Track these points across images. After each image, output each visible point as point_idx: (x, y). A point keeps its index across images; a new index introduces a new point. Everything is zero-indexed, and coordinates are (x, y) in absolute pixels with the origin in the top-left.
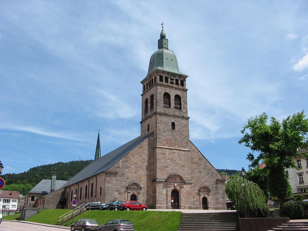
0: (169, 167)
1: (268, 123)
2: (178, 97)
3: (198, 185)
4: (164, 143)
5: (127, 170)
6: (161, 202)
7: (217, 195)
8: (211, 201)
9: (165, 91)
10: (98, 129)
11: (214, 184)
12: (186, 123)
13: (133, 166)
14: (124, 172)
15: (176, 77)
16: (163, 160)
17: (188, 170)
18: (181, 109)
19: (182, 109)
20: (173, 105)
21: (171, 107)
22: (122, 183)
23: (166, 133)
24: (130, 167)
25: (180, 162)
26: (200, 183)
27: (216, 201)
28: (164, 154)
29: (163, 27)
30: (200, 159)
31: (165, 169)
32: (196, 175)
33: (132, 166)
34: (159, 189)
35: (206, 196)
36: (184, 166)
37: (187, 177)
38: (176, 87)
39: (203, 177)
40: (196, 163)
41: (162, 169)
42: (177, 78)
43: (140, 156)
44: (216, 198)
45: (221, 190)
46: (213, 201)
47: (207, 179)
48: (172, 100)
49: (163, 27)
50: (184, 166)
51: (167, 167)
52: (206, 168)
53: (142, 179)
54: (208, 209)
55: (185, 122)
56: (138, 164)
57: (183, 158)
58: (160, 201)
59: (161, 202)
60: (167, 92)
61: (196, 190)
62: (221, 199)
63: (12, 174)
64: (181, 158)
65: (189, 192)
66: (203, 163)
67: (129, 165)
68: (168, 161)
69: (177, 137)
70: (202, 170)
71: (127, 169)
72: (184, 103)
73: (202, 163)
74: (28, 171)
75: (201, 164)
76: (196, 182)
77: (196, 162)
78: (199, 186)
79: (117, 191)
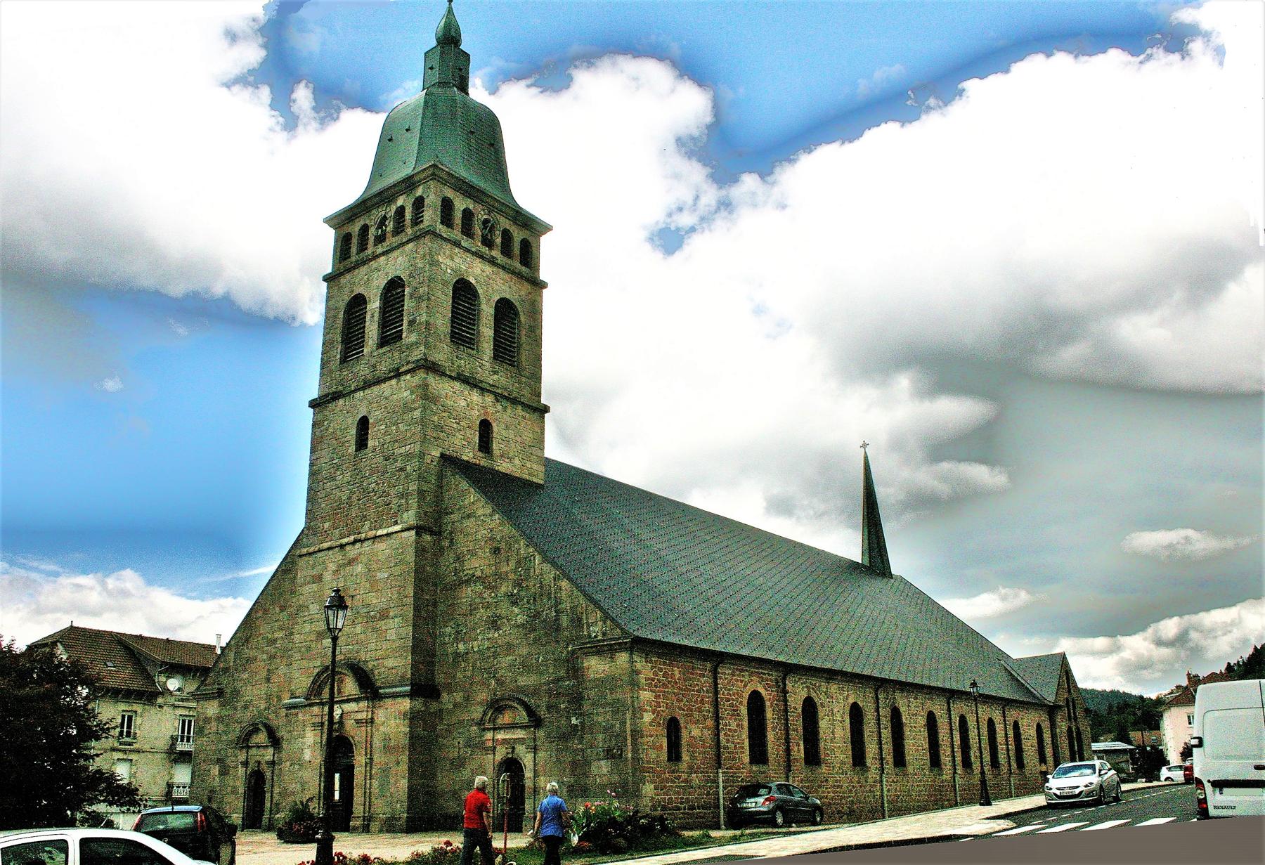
5: (245, 676)
7: (575, 744)
36: (384, 615)
65: (393, 743)
67: (252, 653)
77: (478, 573)
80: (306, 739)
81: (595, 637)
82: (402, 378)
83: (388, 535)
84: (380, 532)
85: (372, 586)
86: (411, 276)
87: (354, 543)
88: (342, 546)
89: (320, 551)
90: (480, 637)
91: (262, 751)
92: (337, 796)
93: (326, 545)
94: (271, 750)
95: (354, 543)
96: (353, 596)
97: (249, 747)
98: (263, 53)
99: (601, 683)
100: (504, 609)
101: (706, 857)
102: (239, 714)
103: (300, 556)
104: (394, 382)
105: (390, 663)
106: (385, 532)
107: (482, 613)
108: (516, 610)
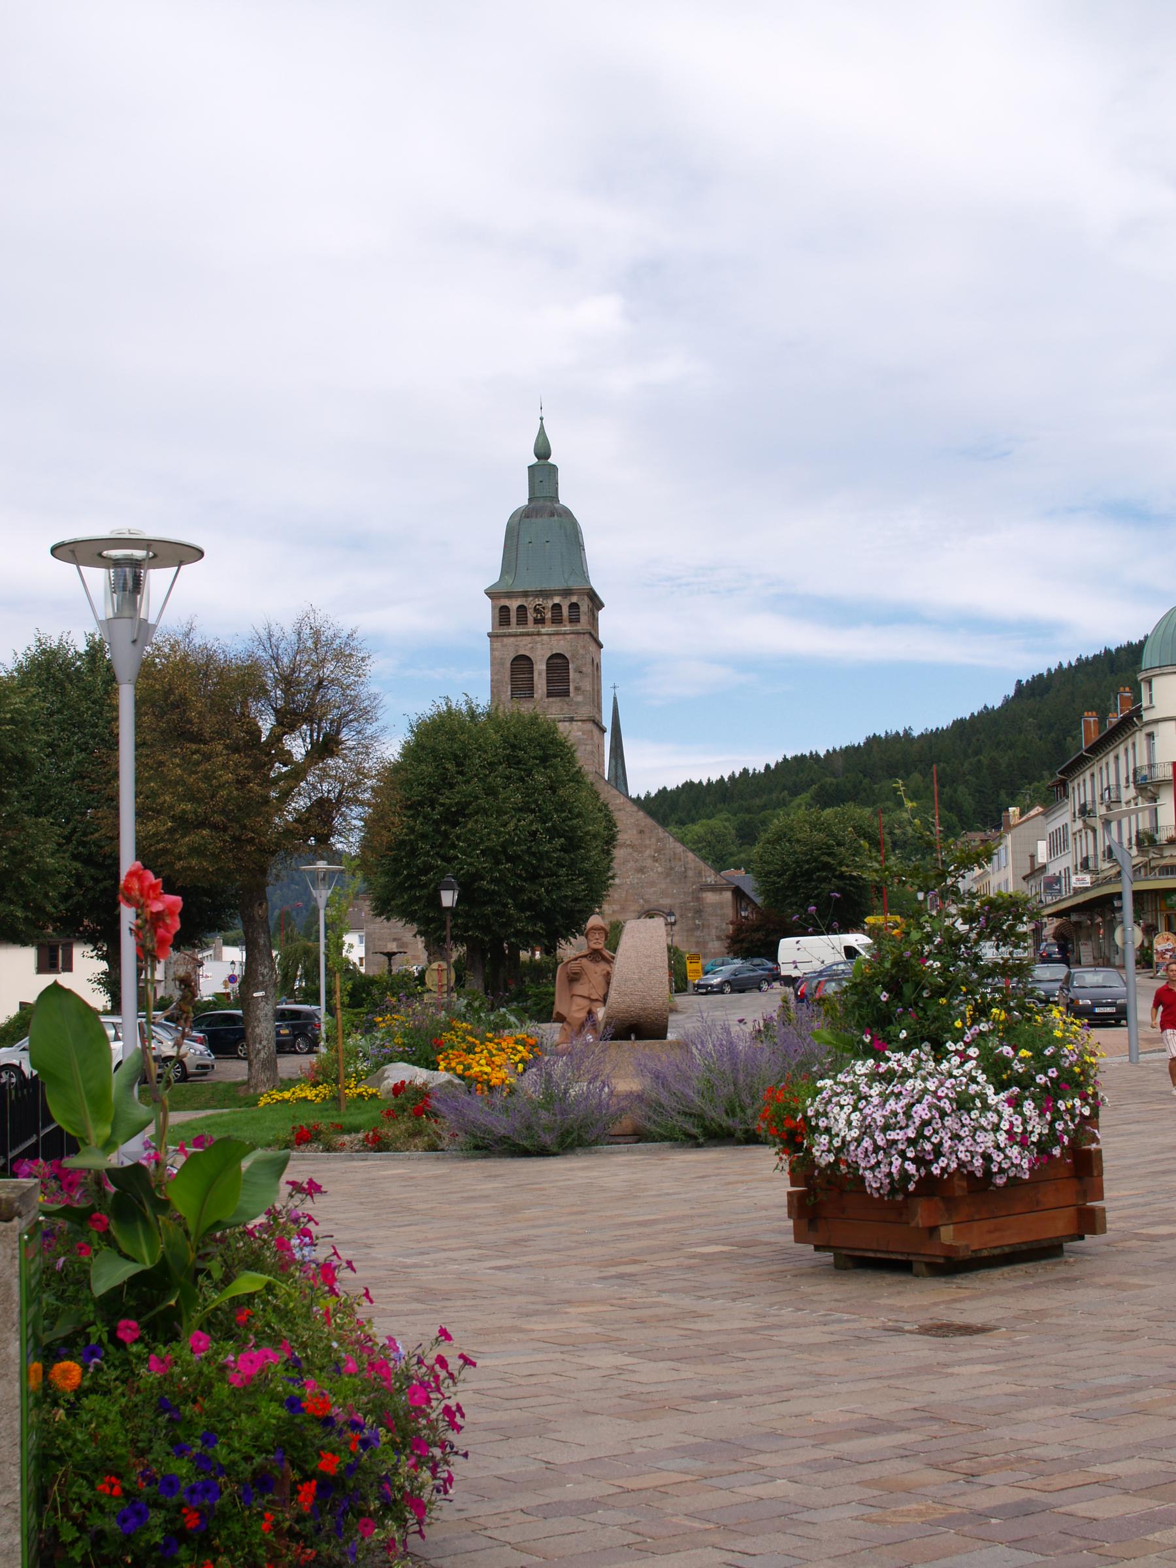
2: (558, 664)
9: (517, 651)
10: (612, 685)
11: (690, 899)
12: (583, 734)
18: (566, 693)
19: (571, 695)
21: (535, 696)
26: (641, 901)
30: (641, 832)
39: (653, 884)
40: (629, 845)
42: (557, 600)
45: (716, 915)
47: (664, 886)
48: (540, 674)
49: (542, 419)
52: (662, 856)
55: (580, 733)
62: (715, 943)
63: (822, 754)
66: (654, 840)
72: (578, 675)
73: (647, 842)
74: (1008, 702)
76: (626, 901)
77: (628, 842)
79: (394, 940)
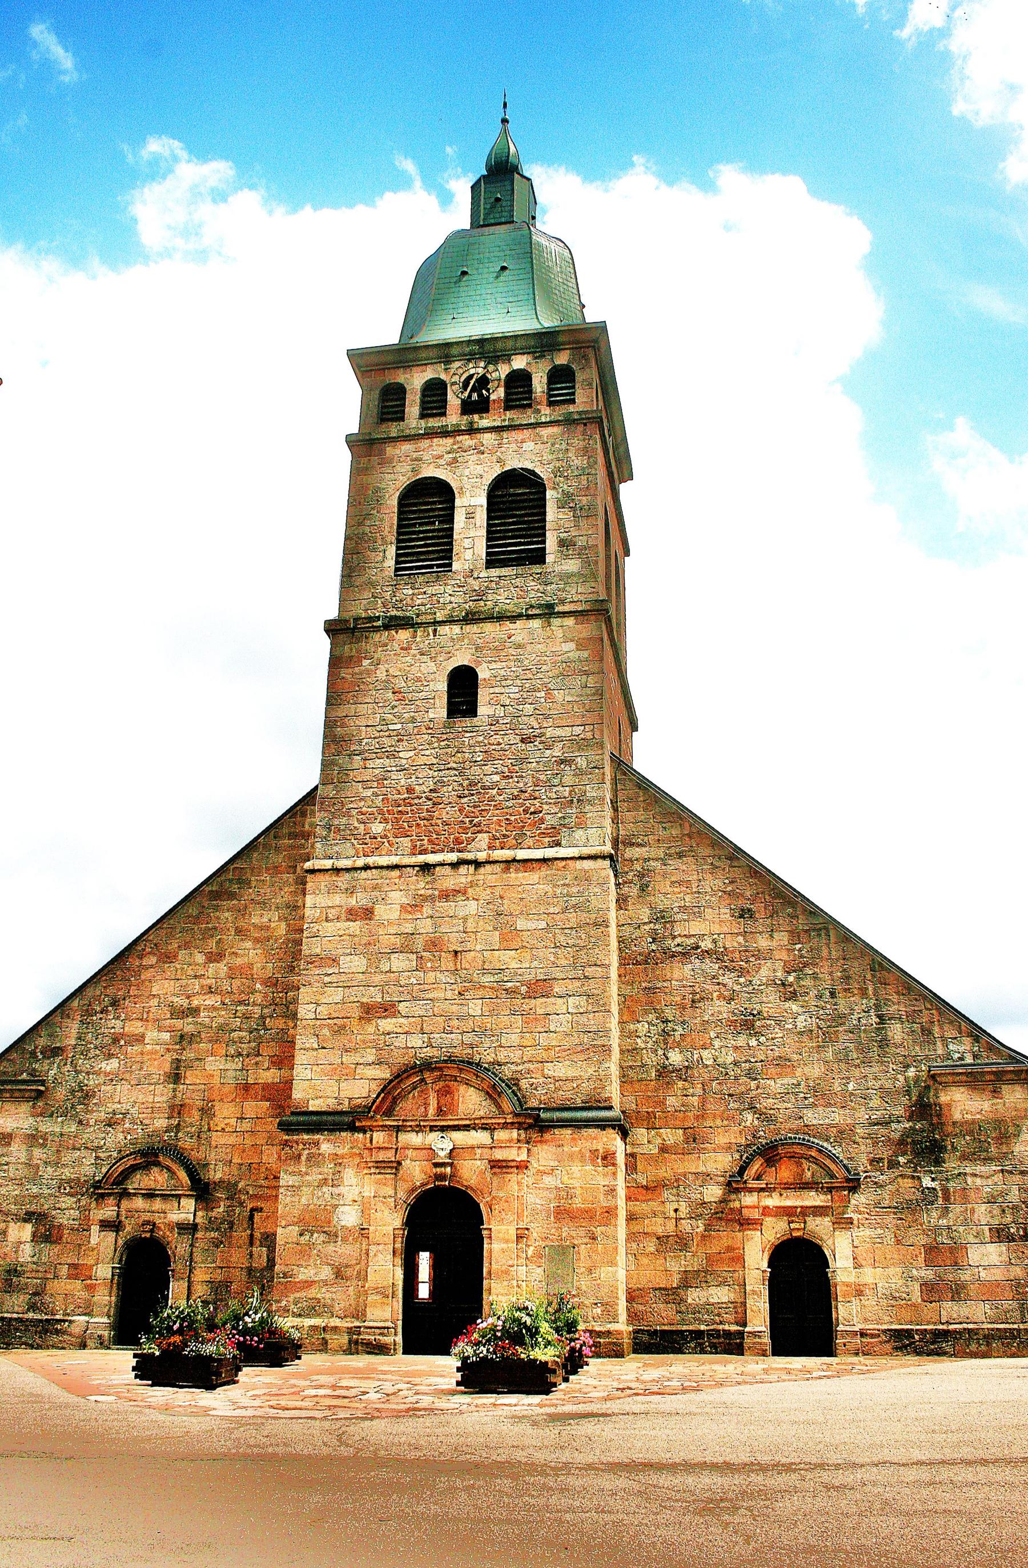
0: (401, 1007)
1: (556, 165)
3: (722, 1139)
4: (377, 828)
5: (112, 1065)
6: (313, 1292)
7: (932, 1217)
8: (869, 1275)
11: (899, 1111)
13: (160, 1030)
14: (92, 1082)
15: (509, 361)
16: (355, 964)
17: (583, 1019)
20: (468, 555)
22: (68, 1157)
23: (392, 755)
24: (140, 1039)
25: (509, 959)
27: (928, 1274)
28: (368, 913)
29: (505, 121)
31: (371, 1029)
32: (705, 1054)
33: (151, 1035)
34: (295, 1189)
35: (819, 1227)
36: (539, 988)
37: (571, 1073)
38: (498, 424)
41: (339, 1031)
42: (519, 363)
43: (214, 957)
44: (923, 1240)
46: (895, 1271)
48: (470, 516)
50: (539, 988)
51: (388, 1009)
53: (219, 1122)
54: (743, 1355)
56: (194, 1011)
57: (531, 925)
58: (309, 1284)
59: (313, 1292)
60: (429, 472)
61: (706, 1177)
64: (521, 924)
65: (578, 1203)
67: (135, 1027)
68: (399, 962)
69: (488, 769)
70: (770, 1002)
71: (110, 1056)
75: (759, 954)
77: (706, 944)
78: (728, 1148)
80: (342, 1190)
81: (961, 1059)
82: (556, 622)
83: (544, 860)
84: (522, 854)
85: (503, 938)
86: (557, 472)
87: (455, 865)
88: (426, 868)
89: (366, 868)
90: (717, 1043)
91: (171, 1205)
92: (424, 1292)
93: (384, 861)
94: (189, 1204)
95: (455, 865)
96: (456, 952)
97: (125, 1194)
98: (721, 167)
99: (972, 1128)
100: (770, 1002)
101: (54, 1352)
102: (91, 1135)
103: (312, 871)
104: (536, 623)
105: (561, 1070)
106: (538, 854)
107: (718, 1008)
108: (795, 1007)
